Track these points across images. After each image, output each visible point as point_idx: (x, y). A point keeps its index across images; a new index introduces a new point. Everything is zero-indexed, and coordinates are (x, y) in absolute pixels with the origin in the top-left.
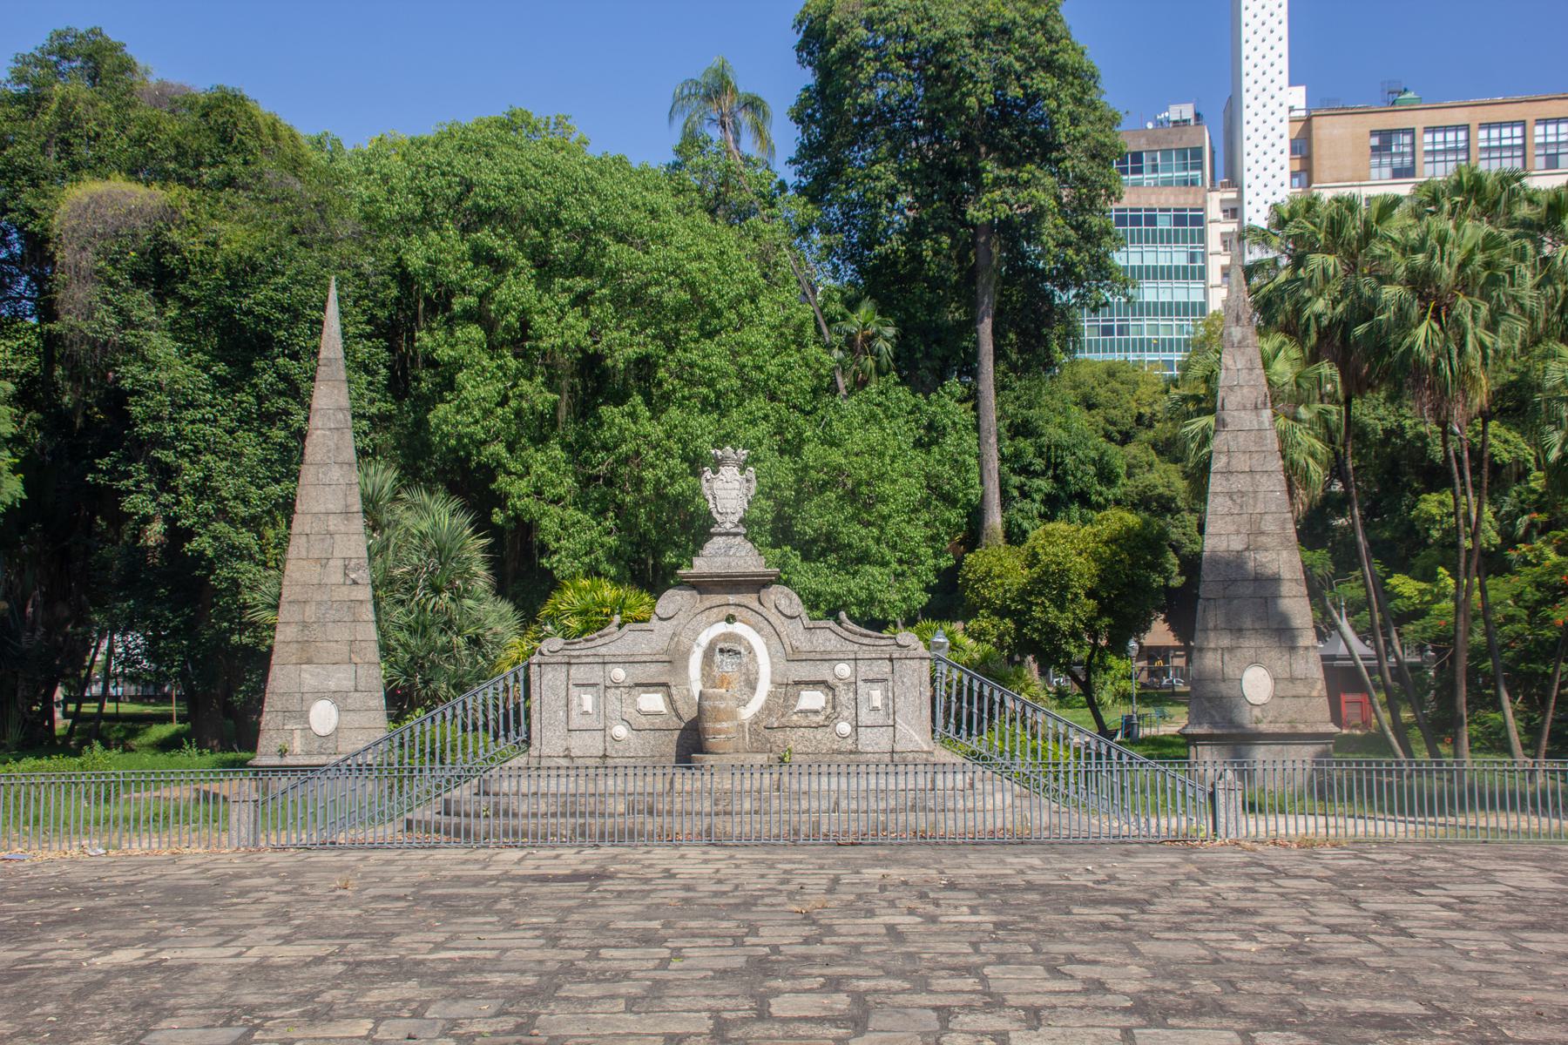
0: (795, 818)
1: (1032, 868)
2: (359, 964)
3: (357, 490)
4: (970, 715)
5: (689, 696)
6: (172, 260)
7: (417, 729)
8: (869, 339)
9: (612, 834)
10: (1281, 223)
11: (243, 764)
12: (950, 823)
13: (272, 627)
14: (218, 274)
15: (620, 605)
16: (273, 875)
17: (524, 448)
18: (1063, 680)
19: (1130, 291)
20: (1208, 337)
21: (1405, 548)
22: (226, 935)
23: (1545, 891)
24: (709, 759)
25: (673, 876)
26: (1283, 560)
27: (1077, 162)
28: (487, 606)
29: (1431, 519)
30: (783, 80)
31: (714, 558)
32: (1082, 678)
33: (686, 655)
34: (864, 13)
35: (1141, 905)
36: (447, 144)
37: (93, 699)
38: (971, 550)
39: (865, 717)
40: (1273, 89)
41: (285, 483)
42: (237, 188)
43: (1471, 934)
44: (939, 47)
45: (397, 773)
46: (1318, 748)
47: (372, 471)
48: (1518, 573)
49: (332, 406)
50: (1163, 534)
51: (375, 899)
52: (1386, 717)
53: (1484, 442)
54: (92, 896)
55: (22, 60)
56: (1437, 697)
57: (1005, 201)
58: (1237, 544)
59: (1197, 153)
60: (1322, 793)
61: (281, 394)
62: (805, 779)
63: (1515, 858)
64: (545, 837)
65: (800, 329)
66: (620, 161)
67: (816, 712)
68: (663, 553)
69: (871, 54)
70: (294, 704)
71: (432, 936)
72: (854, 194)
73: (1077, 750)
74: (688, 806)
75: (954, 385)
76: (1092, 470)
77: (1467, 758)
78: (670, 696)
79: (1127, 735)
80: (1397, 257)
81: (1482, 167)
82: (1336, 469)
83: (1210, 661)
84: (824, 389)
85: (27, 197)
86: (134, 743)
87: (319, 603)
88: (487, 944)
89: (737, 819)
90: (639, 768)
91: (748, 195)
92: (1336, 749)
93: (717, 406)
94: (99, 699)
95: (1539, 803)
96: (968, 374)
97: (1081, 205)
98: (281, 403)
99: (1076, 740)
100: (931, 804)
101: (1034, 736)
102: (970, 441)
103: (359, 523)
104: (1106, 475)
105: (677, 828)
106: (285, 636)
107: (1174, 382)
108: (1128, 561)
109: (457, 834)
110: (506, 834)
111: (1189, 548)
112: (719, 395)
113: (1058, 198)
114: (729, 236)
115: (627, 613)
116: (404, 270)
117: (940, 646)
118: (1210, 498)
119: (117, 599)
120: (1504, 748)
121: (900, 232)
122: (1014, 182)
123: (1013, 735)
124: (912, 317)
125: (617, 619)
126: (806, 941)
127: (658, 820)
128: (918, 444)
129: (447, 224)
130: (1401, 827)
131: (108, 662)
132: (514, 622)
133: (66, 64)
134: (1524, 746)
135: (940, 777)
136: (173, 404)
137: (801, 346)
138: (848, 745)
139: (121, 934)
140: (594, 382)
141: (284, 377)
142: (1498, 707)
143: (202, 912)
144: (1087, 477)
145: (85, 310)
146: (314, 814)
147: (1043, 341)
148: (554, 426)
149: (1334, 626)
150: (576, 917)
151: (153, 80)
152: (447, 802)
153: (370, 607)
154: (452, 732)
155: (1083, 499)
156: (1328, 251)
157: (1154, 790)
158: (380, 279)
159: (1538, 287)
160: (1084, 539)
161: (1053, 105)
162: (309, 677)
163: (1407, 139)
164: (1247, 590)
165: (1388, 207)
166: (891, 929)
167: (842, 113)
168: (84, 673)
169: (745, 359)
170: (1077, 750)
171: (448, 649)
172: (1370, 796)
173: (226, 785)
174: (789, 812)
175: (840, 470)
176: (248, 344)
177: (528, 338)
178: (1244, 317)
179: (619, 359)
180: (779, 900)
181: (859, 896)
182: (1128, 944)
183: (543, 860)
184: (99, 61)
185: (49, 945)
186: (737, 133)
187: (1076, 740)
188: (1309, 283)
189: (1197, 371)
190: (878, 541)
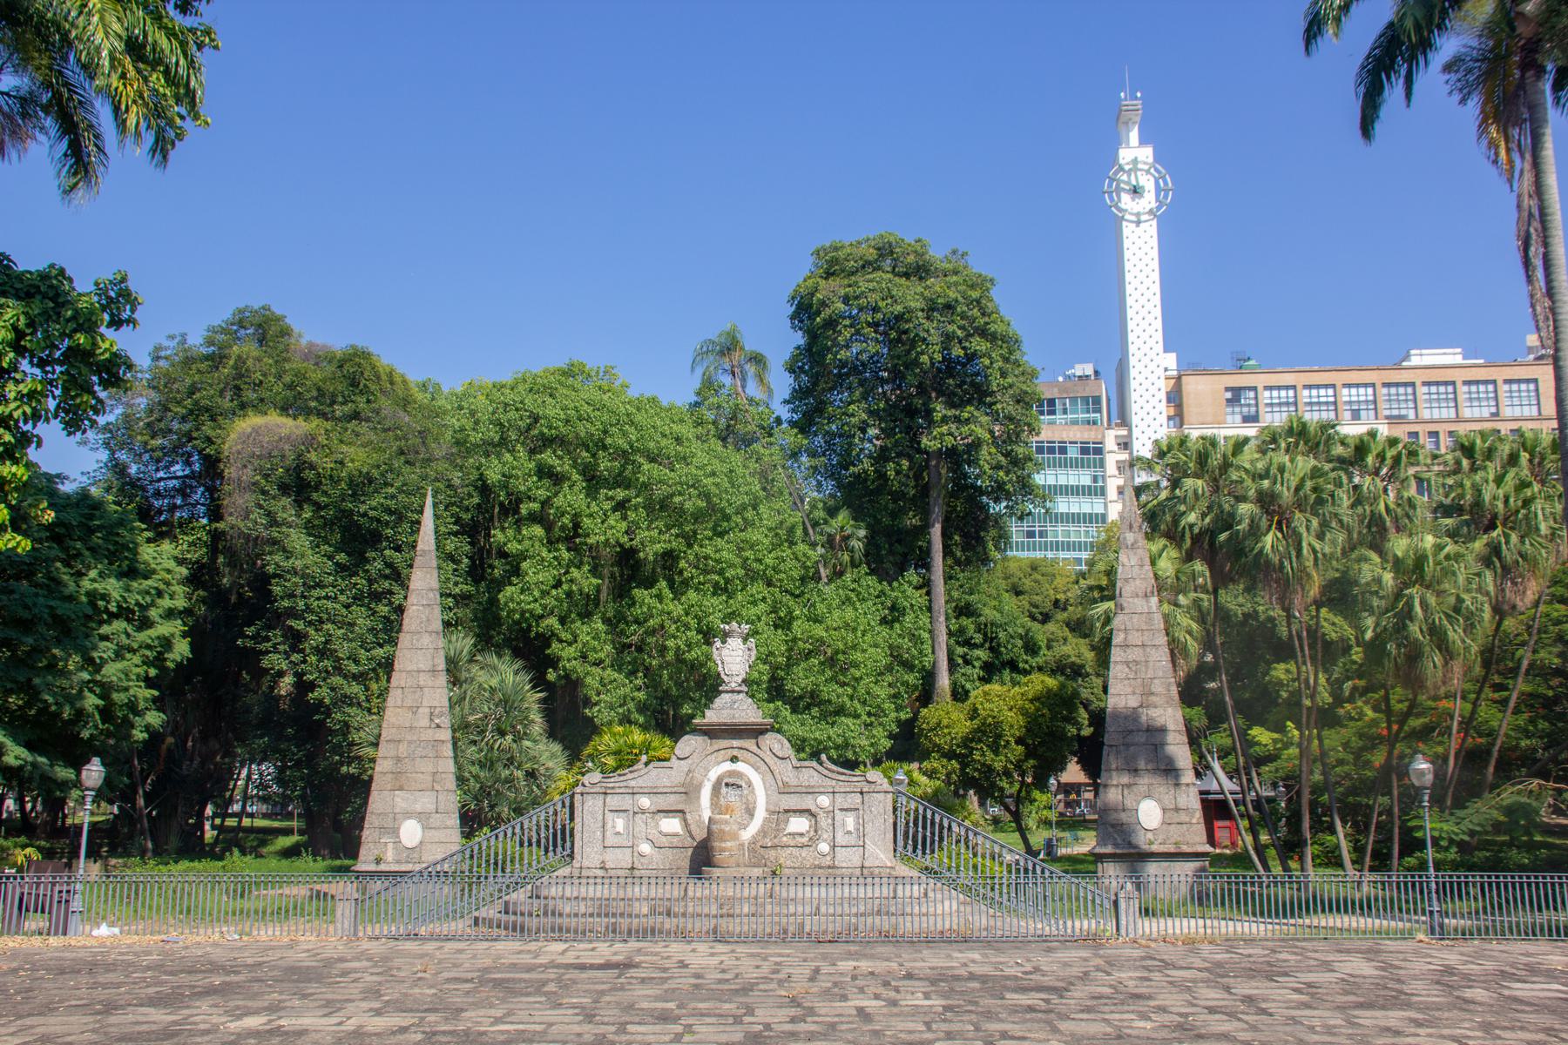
0: (784, 920)
1: (973, 961)
2: (435, 1033)
3: (442, 653)
4: (924, 838)
5: (700, 821)
6: (309, 475)
7: (484, 845)
8: (846, 538)
9: (637, 932)
10: (1162, 454)
11: (347, 869)
12: (908, 925)
13: (373, 760)
14: (343, 485)
15: (646, 747)
16: (369, 960)
17: (573, 622)
18: (996, 810)
19: (1048, 504)
20: (1108, 540)
21: (1262, 705)
22: (331, 1007)
23: (1370, 977)
24: (716, 872)
25: (686, 966)
26: (1169, 715)
27: (1005, 405)
28: (541, 747)
29: (1280, 683)
30: (780, 341)
31: (717, 713)
32: (1013, 808)
33: (699, 787)
34: (842, 292)
35: (1059, 992)
36: (521, 388)
37: (234, 815)
38: (925, 706)
39: (840, 839)
40: (1152, 354)
41: (387, 648)
42: (361, 420)
43: (1315, 1013)
44: (899, 318)
45: (469, 876)
46: (1198, 864)
47: (454, 638)
48: (1342, 726)
49: (425, 589)
50: (1076, 694)
51: (449, 980)
52: (1249, 839)
53: (1318, 623)
54: (228, 973)
55: (212, 330)
56: (1288, 823)
57: (951, 434)
58: (1133, 702)
59: (1097, 400)
60: (1201, 899)
61: (386, 577)
62: (792, 888)
63: (1348, 951)
64: (584, 932)
65: (791, 530)
66: (653, 401)
67: (802, 835)
68: (681, 705)
69: (847, 322)
70: (389, 823)
71: (493, 1012)
72: (834, 427)
73: (1009, 866)
74: (699, 910)
75: (912, 576)
76: (1020, 643)
77: (1311, 871)
78: (685, 820)
79: (1048, 854)
80: (1248, 482)
81: (1307, 417)
82: (1208, 644)
83: (1112, 795)
84: (810, 577)
85: (207, 429)
86: (265, 850)
87: (410, 742)
88: (537, 1019)
89: (738, 920)
90: (659, 878)
91: (752, 427)
92: (1211, 865)
93: (725, 590)
94: (239, 815)
95: (1365, 907)
96: (923, 566)
97: (1009, 437)
98: (387, 584)
99: (1008, 857)
100: (893, 909)
101: (975, 855)
102: (924, 619)
103: (443, 679)
104: (1031, 648)
105: (690, 927)
106: (383, 767)
107: (1083, 575)
108: (1048, 715)
109: (514, 929)
110: (553, 930)
111: (1096, 705)
112: (727, 581)
113: (991, 432)
114: (737, 459)
115: (652, 753)
116: (484, 482)
117: (901, 782)
118: (1112, 665)
119: (255, 737)
120: (1339, 864)
121: (870, 456)
122: (957, 419)
123: (958, 854)
124: (879, 522)
125: (644, 758)
126: (793, 1020)
127: (675, 920)
128: (884, 621)
129: (519, 447)
130: (1262, 927)
131: (247, 786)
132: (562, 759)
133: (242, 331)
134: (1353, 862)
135: (900, 887)
136: (304, 584)
137: (792, 544)
138: (827, 861)
139: (250, 1004)
140: (629, 569)
141: (389, 565)
142: (1333, 832)
143: (312, 988)
144: (1016, 649)
145: (243, 512)
146: (402, 911)
147: (981, 541)
148: (597, 605)
149: (1208, 767)
150: (608, 998)
151: (304, 342)
152: (507, 903)
153: (450, 746)
154: (512, 847)
155: (1013, 666)
156: (1197, 476)
157: (1070, 898)
158: (466, 490)
159: (1353, 506)
160: (1013, 698)
161: (987, 362)
162: (401, 801)
163: (1252, 394)
164: (1141, 738)
165: (1240, 445)
166: (861, 1011)
167: (825, 366)
168: (228, 794)
169: (748, 553)
170: (1009, 866)
171: (510, 781)
172: (1238, 902)
173: (334, 885)
174: (779, 914)
175: (822, 641)
176: (362, 539)
177: (579, 536)
178: (1136, 525)
179: (650, 553)
180: (771, 986)
181: (835, 984)
182: (1049, 1023)
183: (583, 952)
184: (266, 329)
185: (195, 1011)
186: (744, 380)
187: (1008, 858)
188: (1183, 500)
189: (1101, 566)
190: (851, 698)
